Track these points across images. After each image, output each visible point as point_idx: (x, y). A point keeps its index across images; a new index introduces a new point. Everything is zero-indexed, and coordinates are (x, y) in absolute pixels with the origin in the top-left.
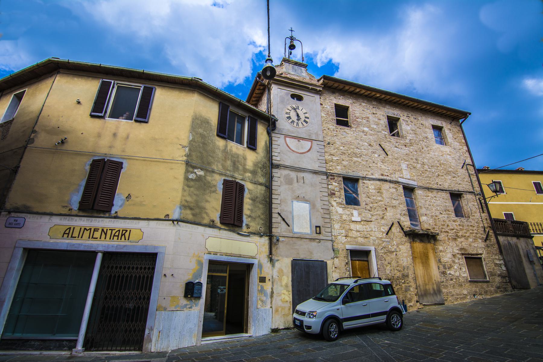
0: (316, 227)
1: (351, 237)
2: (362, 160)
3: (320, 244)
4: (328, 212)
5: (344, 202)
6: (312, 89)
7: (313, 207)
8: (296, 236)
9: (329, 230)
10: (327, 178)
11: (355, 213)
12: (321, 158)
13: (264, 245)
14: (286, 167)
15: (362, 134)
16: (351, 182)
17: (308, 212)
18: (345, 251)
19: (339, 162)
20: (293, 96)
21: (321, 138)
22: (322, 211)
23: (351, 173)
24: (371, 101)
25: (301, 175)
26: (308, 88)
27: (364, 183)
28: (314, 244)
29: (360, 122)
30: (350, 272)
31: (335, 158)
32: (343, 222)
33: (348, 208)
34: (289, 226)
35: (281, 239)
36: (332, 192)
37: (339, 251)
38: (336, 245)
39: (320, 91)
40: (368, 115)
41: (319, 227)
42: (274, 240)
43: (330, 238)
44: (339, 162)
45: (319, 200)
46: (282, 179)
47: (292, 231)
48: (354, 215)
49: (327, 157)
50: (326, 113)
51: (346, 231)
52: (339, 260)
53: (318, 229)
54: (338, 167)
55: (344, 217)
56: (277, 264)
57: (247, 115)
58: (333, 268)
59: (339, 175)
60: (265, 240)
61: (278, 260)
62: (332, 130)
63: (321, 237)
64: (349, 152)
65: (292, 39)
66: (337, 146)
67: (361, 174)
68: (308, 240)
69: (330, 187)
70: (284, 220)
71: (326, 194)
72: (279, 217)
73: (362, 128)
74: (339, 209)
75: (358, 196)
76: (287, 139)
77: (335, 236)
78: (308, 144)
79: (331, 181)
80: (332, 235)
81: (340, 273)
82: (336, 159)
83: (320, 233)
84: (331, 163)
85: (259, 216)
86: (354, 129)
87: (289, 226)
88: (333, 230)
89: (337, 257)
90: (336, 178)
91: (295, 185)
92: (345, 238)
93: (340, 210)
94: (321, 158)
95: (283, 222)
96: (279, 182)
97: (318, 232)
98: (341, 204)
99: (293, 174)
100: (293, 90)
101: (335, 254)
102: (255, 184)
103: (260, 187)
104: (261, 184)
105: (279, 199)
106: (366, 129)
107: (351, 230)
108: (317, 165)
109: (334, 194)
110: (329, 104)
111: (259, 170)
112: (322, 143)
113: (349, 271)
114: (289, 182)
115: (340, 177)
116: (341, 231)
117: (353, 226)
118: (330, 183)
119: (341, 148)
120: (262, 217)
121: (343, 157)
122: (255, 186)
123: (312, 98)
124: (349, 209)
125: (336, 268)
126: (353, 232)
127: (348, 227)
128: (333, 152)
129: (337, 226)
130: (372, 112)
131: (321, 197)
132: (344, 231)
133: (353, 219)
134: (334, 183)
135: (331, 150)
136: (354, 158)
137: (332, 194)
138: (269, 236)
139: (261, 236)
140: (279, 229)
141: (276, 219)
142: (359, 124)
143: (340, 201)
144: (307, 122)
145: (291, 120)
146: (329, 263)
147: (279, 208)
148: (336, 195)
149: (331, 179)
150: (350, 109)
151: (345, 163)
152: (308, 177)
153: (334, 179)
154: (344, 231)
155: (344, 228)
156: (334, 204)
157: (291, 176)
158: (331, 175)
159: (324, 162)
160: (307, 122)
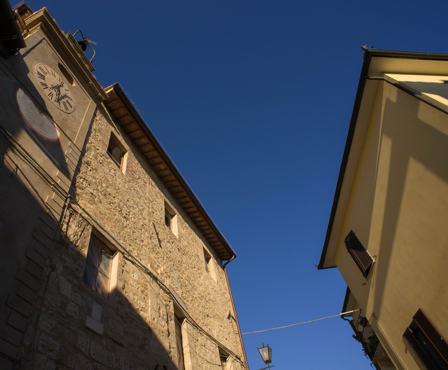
26: (87, 82)
145: (43, 81)
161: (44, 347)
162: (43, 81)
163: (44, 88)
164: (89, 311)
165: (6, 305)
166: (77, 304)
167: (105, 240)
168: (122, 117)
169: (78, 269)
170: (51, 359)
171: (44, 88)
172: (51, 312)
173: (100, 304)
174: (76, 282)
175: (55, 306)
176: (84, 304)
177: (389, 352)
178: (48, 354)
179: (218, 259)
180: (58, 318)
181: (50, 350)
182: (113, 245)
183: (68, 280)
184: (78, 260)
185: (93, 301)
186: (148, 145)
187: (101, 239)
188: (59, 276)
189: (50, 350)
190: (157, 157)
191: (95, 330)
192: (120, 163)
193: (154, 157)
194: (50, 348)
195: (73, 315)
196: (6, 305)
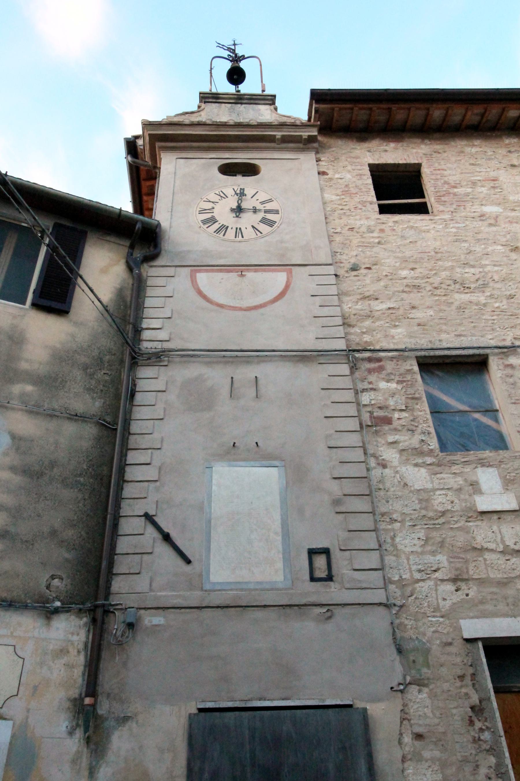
0: (312, 553)
1: (481, 582)
2: (491, 296)
3: (330, 626)
4: (362, 489)
5: (434, 444)
6: (285, 140)
7: (297, 474)
8: (216, 599)
9: (372, 560)
10: (354, 368)
11: (488, 478)
12: (326, 311)
13: (63, 652)
14: (189, 356)
15: (477, 224)
16: (457, 367)
17: (276, 499)
18: (458, 647)
19: (394, 316)
20: (228, 170)
21: (324, 256)
22: (335, 488)
23: (453, 338)
24: (500, 137)
25: (246, 373)
26: (271, 139)
27: (511, 366)
28: (307, 627)
29: (467, 195)
30: (499, 756)
31: (379, 306)
32: (433, 521)
33: (454, 463)
34: (188, 562)
35: (152, 620)
36: (379, 413)
37: (427, 652)
38: (409, 623)
39: (311, 139)
40: (492, 174)
41: (326, 552)
42: (116, 625)
43: (380, 596)
44: (394, 316)
45: (321, 448)
46: (172, 397)
47: (197, 582)
48: (484, 487)
49: (350, 306)
50: (339, 192)
51: (453, 557)
52: (433, 696)
53: (320, 561)
54: (393, 331)
55: (440, 501)
56: (120, 742)
57: (47, 223)
58: (407, 739)
59: (401, 353)
60: (69, 631)
61: (126, 719)
62: (364, 229)
63: (333, 593)
64: (436, 281)
65: (236, 59)
66: (386, 270)
67: (489, 340)
68: (271, 614)
69: (365, 399)
70: (167, 538)
71: (353, 424)
72: (151, 530)
73: (477, 208)
74: (409, 472)
75: (497, 420)
76: (202, 278)
77: (402, 584)
78: (280, 279)
79: (372, 378)
80: (387, 582)
81: (444, 765)
82: (384, 306)
83: (330, 578)
84: (367, 323)
85: (53, 533)
86: (447, 216)
87: (188, 562)
88: (389, 560)
89: (420, 683)
90: (389, 366)
91: (225, 406)
92: (450, 587)
93: (419, 477)
94: (326, 311)
95: (163, 550)
96: (160, 406)
97: (321, 572)
98: (419, 452)
99: (217, 376)
100: (227, 155)
101: (409, 664)
102: (51, 416)
103: (70, 429)
104: (76, 417)
105: (156, 462)
106: (491, 209)
107: (482, 550)
108: (311, 336)
109: (388, 421)
110: (349, 168)
111: (78, 374)
112: (331, 270)
113: (491, 751)
114: (200, 400)
115: (405, 359)
116: (430, 559)
117: (483, 534)
118: (361, 386)
119: (404, 273)
120: (70, 534)
121: (414, 298)
122: (52, 425)
123: (289, 164)
124: (455, 469)
125: (419, 736)
126: (488, 556)
127: (461, 539)
128: (371, 289)
129: (408, 541)
130: (506, 162)
131: (328, 437)
132: (442, 559)
133: (483, 504)
134: (383, 385)
135: (367, 283)
136: (457, 296)
137: (378, 422)
138: (92, 610)
139: (50, 614)
140: (143, 576)
141: (133, 535)
142: (461, 202)
143: (415, 441)
144: (271, 223)
145: (216, 226)
146: (383, 714)
147: (153, 497)
148: (396, 424)
149: (370, 371)
150: (425, 171)
151: (419, 315)
152: (276, 376)
153: (381, 369)
154: (442, 559)
155: (442, 544)
156: (390, 455)
157: (209, 383)
158: (370, 360)
159: (339, 321)
160: (271, 223)
161: (423, 571)
162: (216, 226)
163: (224, 235)
164: (475, 487)
165: (341, 550)
166: (448, 489)
167: (452, 359)
168: (369, 121)
169: (423, 441)
170: (442, 580)
171: (224, 235)
172: (410, 524)
173: (490, 466)
174: (429, 460)
175: (412, 512)
176: (461, 482)
177: (120, 399)
178: (435, 577)
179: (118, 211)
180: (426, 524)
181: (435, 571)
182: (473, 356)
183: (416, 465)
184: (417, 427)
185: (476, 467)
186: (450, 112)
187: (448, 361)
188: (398, 469)
189: (435, 571)
190: (486, 110)
191: (499, 508)
192: (52, 255)
193: (483, 115)
194: (433, 569)
195: (449, 507)
196: (341, 550)
